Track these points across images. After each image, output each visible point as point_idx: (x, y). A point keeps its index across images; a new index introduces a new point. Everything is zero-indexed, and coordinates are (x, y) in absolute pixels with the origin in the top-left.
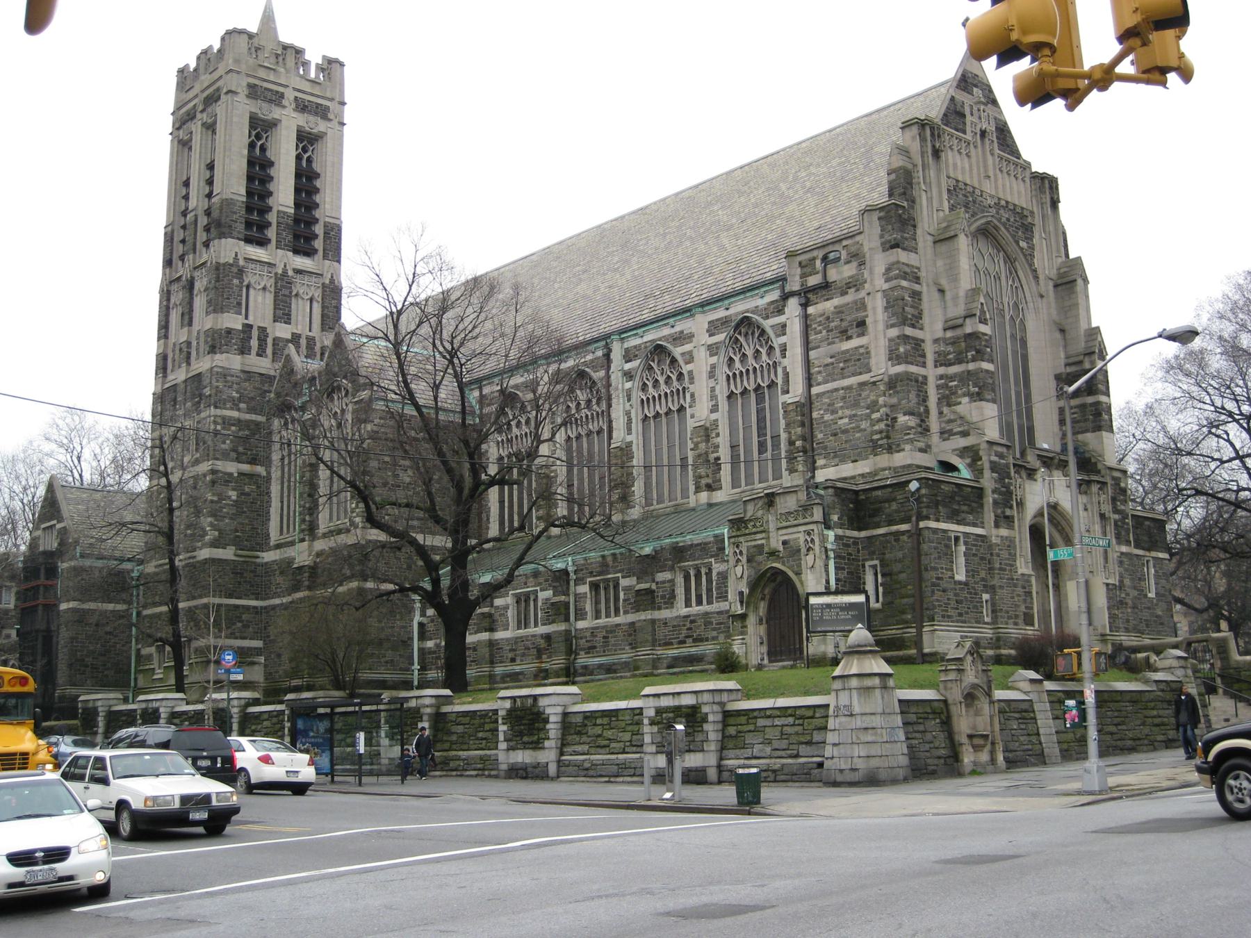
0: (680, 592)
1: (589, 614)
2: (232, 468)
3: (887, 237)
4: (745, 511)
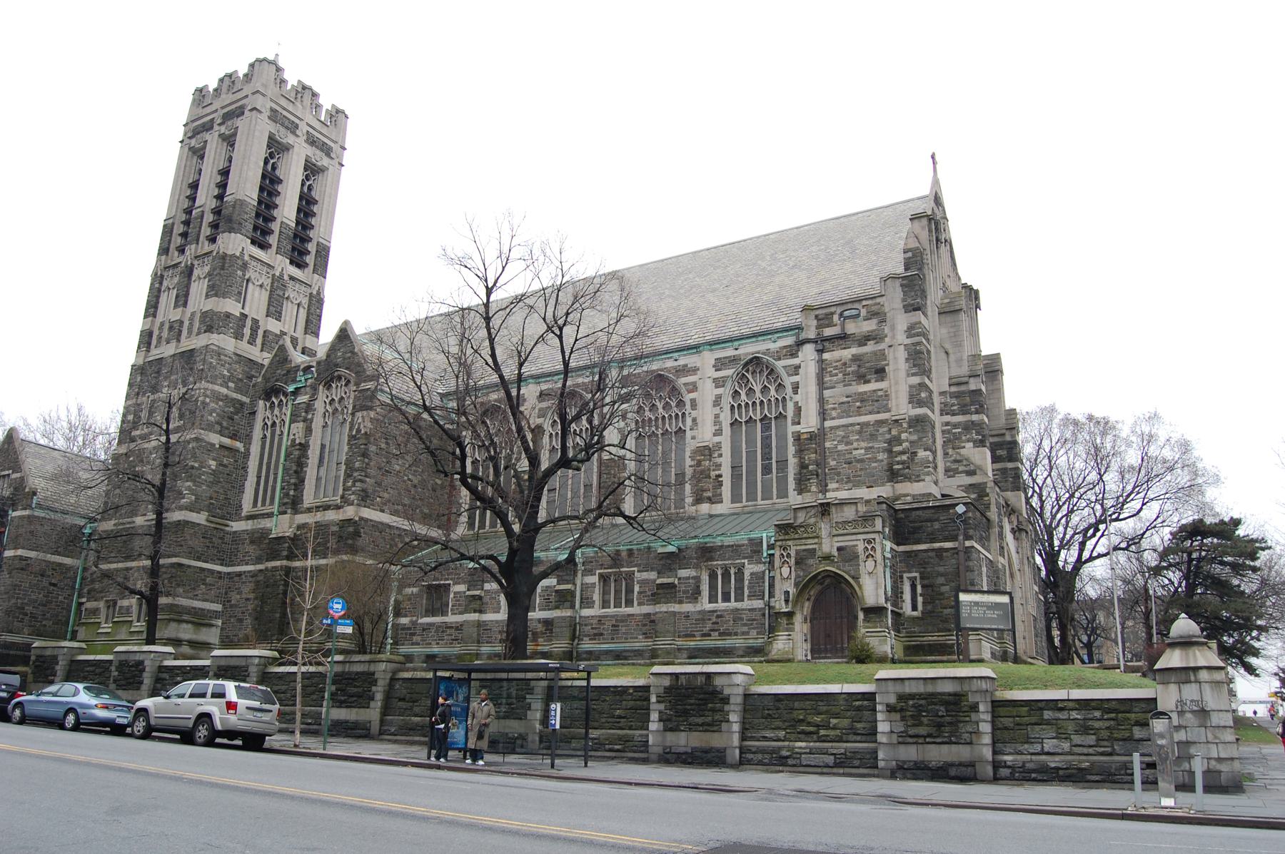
1: (597, 603)
2: (215, 439)
4: (795, 518)
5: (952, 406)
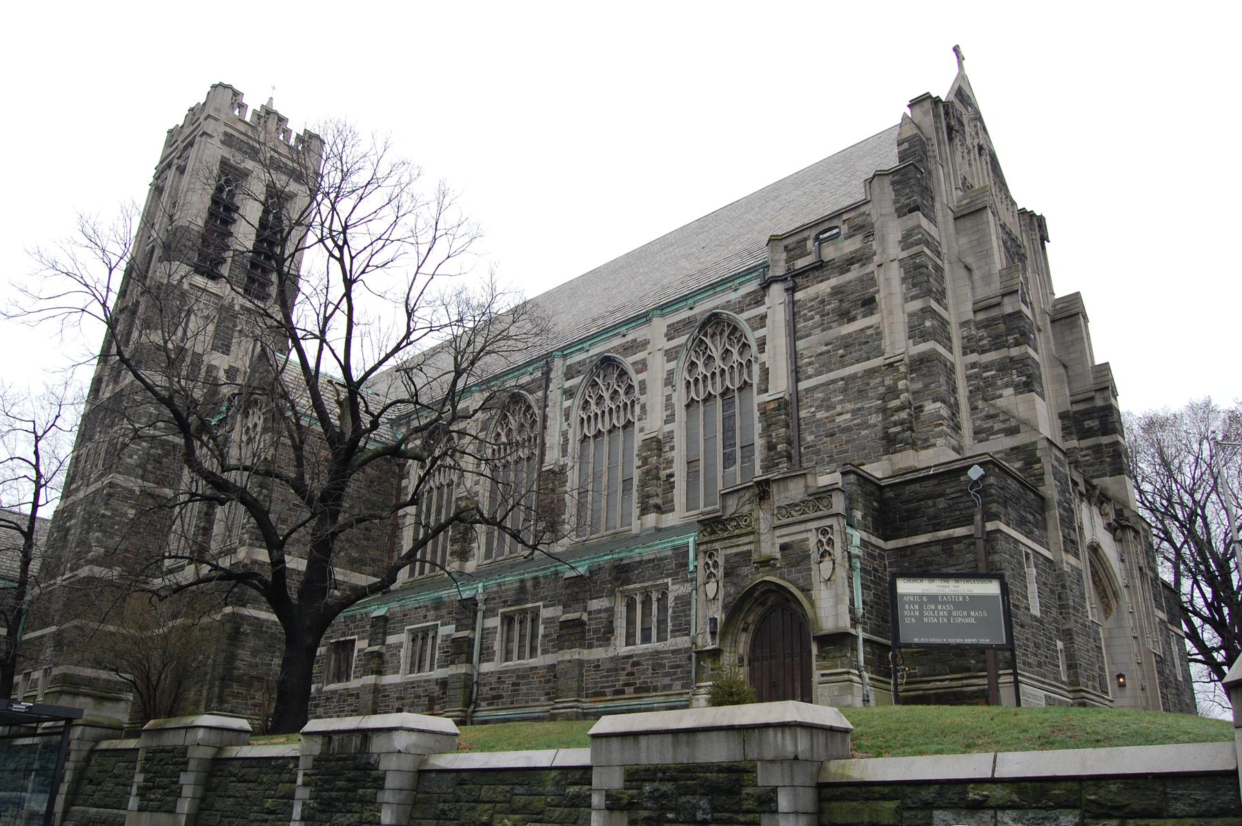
0: (620, 625)
3: (903, 200)
4: (724, 508)
5: (980, 340)
